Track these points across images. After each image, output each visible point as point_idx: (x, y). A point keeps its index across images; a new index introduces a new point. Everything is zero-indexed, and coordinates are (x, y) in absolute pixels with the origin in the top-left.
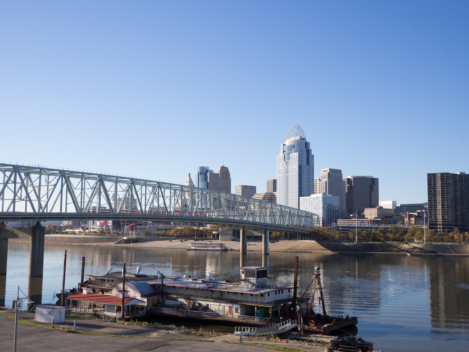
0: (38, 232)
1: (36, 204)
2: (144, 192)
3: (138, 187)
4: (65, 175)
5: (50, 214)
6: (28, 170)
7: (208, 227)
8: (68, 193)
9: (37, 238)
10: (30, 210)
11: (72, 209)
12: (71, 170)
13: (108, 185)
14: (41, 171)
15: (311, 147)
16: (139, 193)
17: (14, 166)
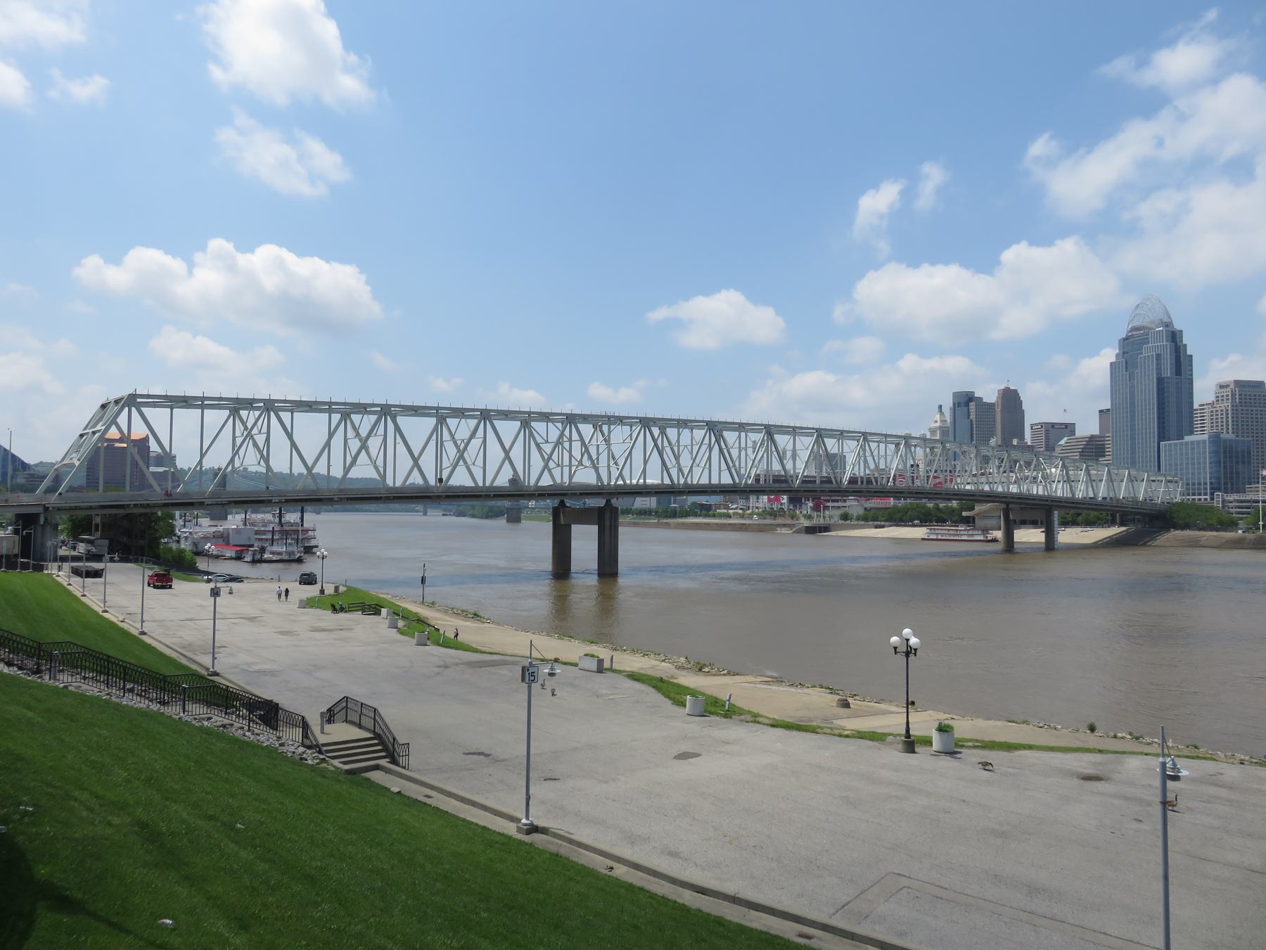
0: (608, 516)
1: (674, 472)
2: (882, 453)
3: (874, 445)
4: (715, 428)
5: (491, 488)
6: (664, 424)
7: (955, 504)
8: (432, 444)
9: (607, 523)
10: (667, 481)
11: (726, 480)
12: (778, 423)
13: (782, 440)
14: (682, 424)
15: (1186, 340)
16: (875, 454)
17: (482, 411)
